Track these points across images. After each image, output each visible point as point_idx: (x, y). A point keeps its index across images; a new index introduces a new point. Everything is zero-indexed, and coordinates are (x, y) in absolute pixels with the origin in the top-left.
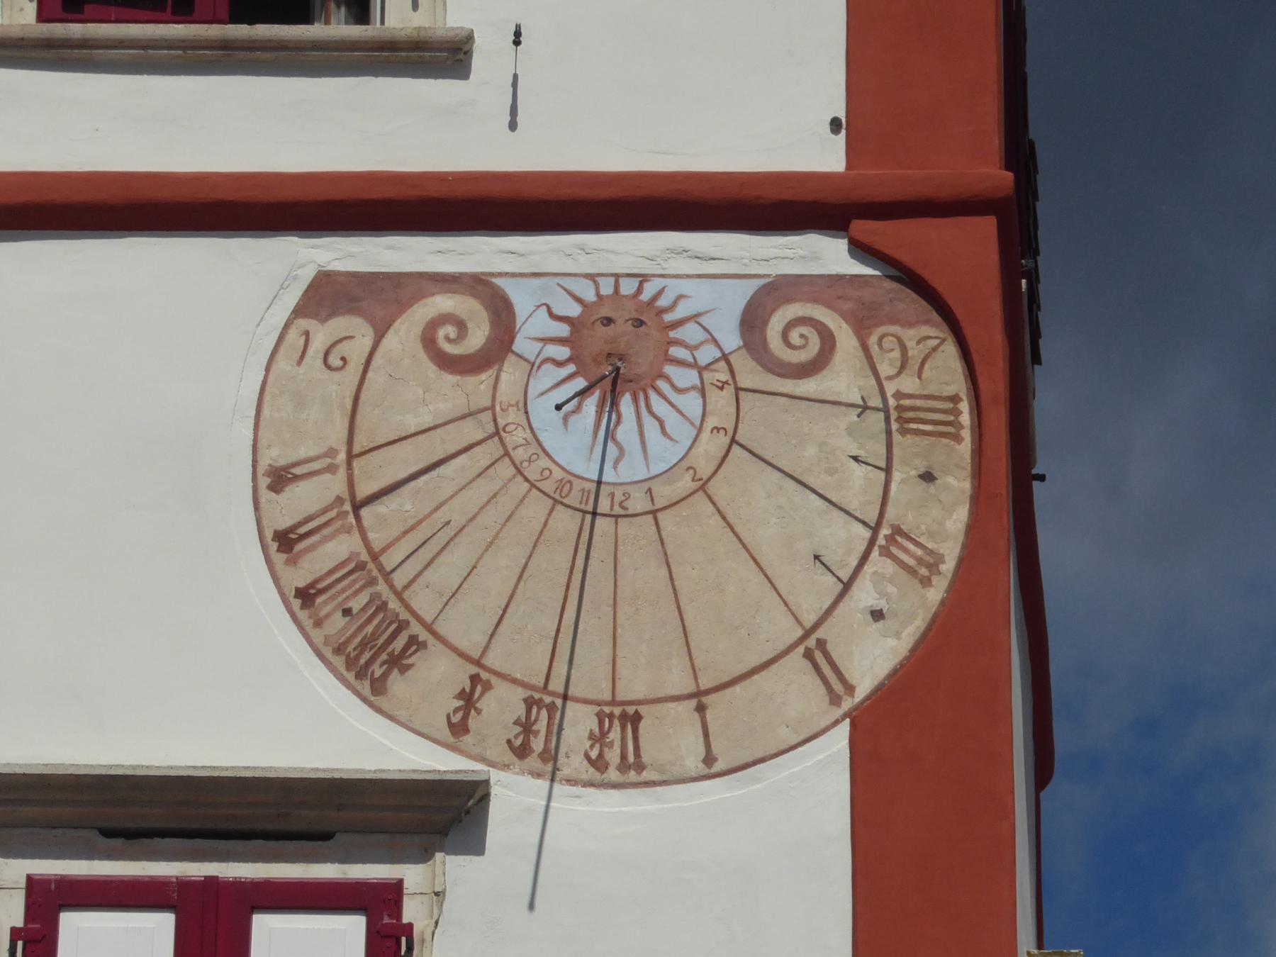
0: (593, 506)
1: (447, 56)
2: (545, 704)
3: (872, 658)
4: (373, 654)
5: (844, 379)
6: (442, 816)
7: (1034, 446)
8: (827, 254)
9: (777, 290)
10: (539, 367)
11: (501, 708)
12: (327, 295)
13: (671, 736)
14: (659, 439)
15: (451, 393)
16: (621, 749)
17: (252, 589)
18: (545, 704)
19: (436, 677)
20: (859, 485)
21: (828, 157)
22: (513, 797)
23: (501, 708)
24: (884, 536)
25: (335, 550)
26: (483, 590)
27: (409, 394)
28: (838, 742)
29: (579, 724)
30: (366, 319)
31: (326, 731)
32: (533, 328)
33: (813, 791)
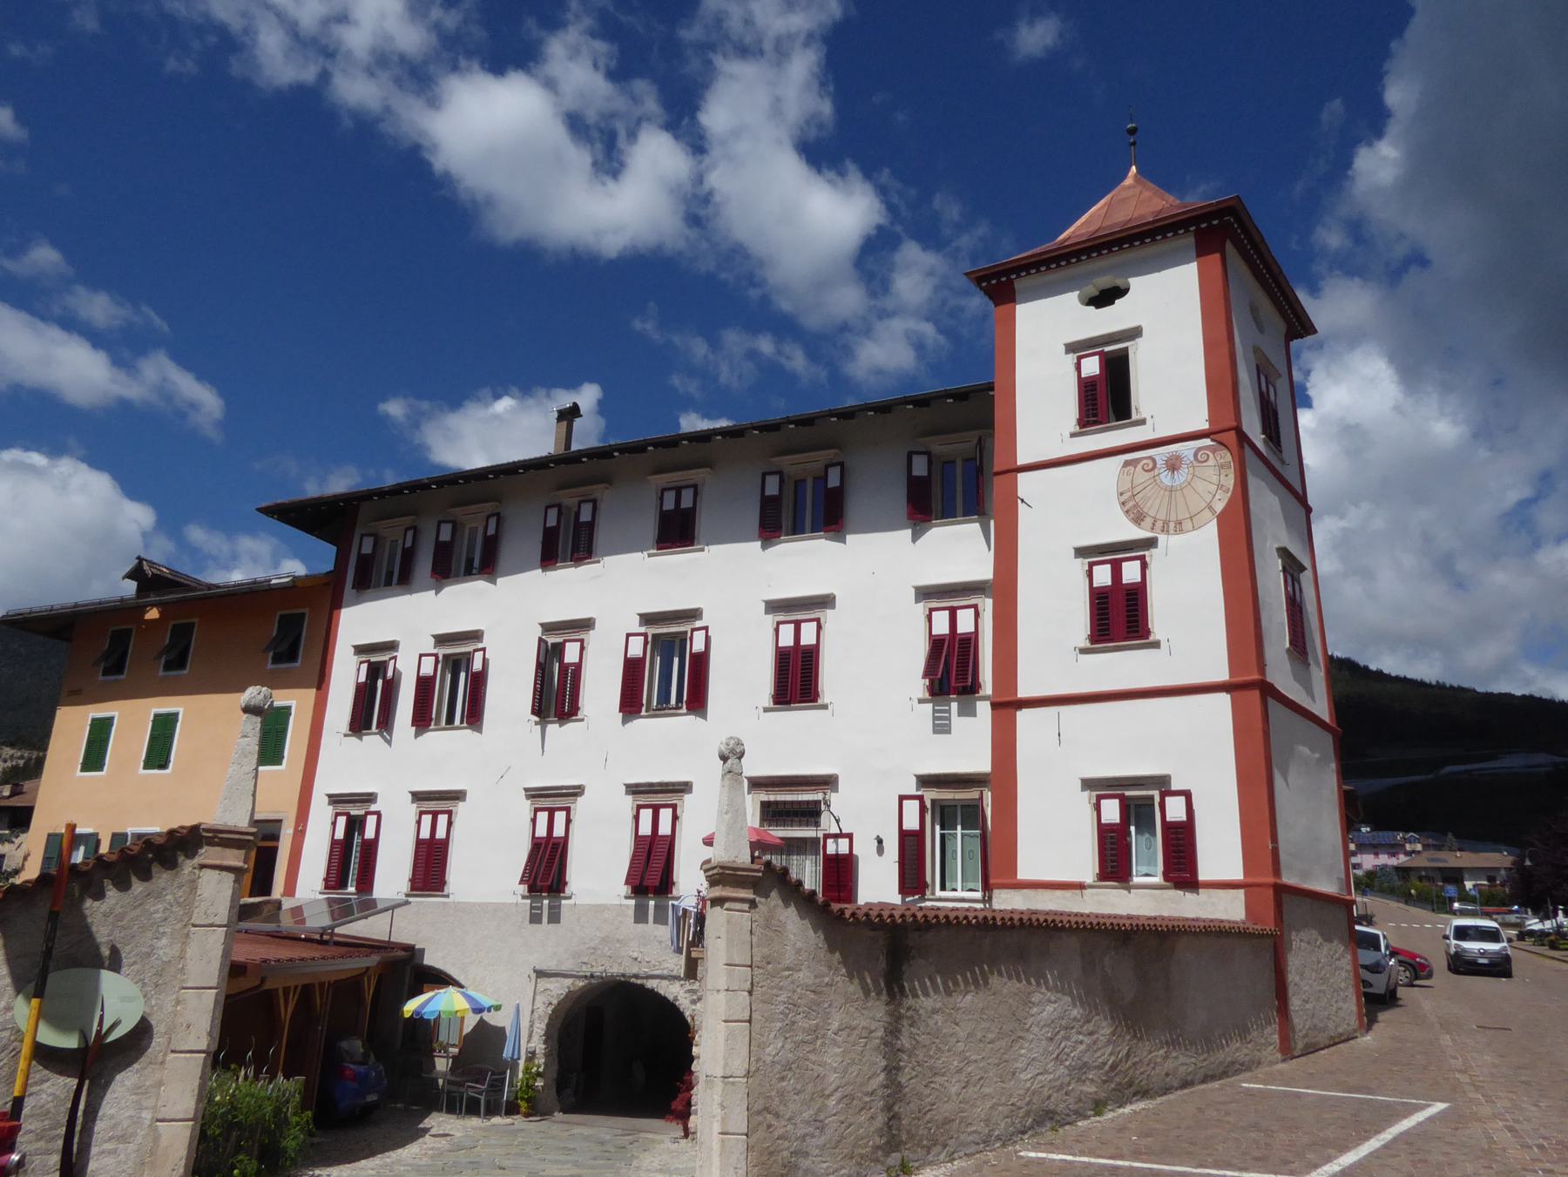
2: (1166, 523)
3: (1219, 507)
4: (1138, 519)
5: (1211, 462)
6: (1151, 543)
8: (1207, 442)
9: (1200, 449)
11: (1159, 524)
13: (1187, 525)
16: (1179, 528)
19: (1149, 521)
20: (1215, 479)
22: (1162, 539)
23: (1159, 524)
24: (1220, 486)
26: (1155, 506)
27: (1141, 477)
28: (1215, 521)
29: (1172, 525)
32: (1159, 462)
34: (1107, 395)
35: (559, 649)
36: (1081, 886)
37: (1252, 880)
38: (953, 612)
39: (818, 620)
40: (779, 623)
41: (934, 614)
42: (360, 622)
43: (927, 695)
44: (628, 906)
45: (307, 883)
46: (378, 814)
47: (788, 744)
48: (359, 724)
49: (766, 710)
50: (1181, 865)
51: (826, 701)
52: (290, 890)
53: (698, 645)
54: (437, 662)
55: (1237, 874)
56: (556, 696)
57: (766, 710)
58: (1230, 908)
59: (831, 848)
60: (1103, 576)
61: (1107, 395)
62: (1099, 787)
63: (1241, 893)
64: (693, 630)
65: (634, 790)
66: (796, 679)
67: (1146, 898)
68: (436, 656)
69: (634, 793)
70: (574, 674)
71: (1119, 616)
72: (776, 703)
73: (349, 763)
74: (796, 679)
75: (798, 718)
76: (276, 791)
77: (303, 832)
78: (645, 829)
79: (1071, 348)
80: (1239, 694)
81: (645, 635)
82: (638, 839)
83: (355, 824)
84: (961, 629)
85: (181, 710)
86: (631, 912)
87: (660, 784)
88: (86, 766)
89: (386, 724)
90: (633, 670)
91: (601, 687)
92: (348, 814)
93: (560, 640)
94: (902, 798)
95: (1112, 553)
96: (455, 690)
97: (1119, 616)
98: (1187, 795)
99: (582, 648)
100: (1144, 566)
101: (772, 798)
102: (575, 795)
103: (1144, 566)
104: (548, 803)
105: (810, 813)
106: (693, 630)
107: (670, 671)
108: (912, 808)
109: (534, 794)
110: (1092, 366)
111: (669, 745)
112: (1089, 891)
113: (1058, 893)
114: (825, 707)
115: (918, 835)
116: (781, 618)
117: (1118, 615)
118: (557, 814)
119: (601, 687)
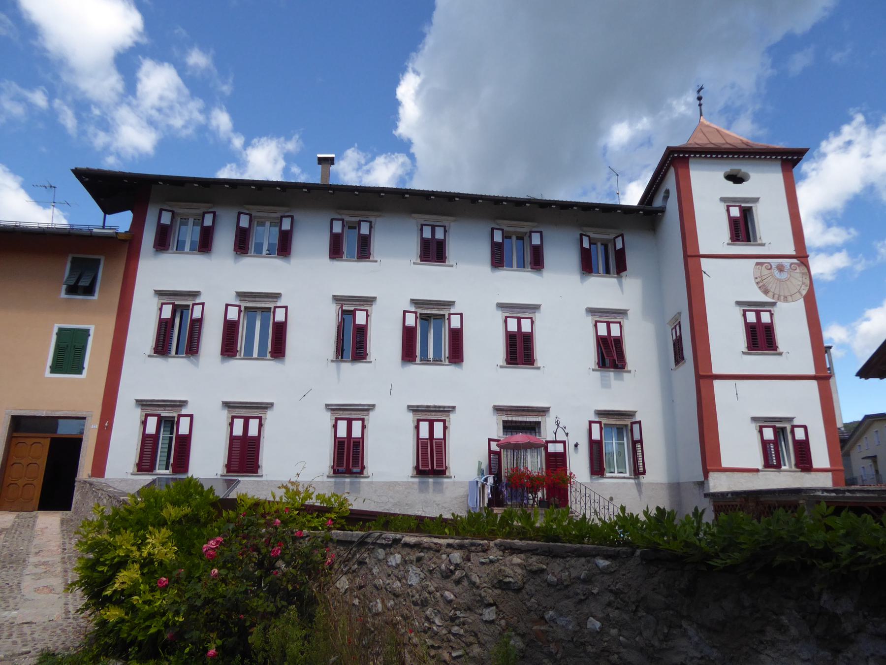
0: (780, 280)
1: (763, 245)
2: (779, 296)
3: (804, 293)
4: (766, 292)
5: (798, 271)
6: (773, 304)
7: (99, 170)
8: (795, 261)
9: (792, 264)
10: (13, 525)
11: (776, 296)
12: (757, 264)
13: (789, 299)
14: (784, 276)
15: (768, 272)
16: (786, 299)
17: (756, 287)
18: (779, 296)
19: (771, 294)
20: (800, 279)
21: (794, 253)
22: (779, 304)
23: (776, 296)
24: (803, 283)
25: (761, 284)
26: (772, 287)
27: (765, 272)
28: (802, 299)
29: (782, 298)
30: (176, 67)
31: (762, 298)
32: (774, 267)
33: (801, 302)
34: (742, 228)
35: (353, 313)
36: (757, 471)
37: (834, 468)
38: (519, 320)
39: (367, 311)
40: (506, 317)
41: (164, 306)
42: (159, 273)
43: (597, 367)
44: (413, 483)
45: (207, 462)
46: (639, 422)
47: (521, 388)
48: (162, 348)
49: (501, 367)
50: (804, 460)
51: (629, 369)
52: (99, 468)
53: (197, 314)
54: (240, 311)
55: (827, 465)
56: (352, 343)
57: (501, 367)
58: (825, 481)
59: (552, 448)
60: (751, 317)
61: (742, 228)
62: (762, 423)
63: (830, 474)
64: (275, 307)
65: (414, 409)
66: (520, 350)
67: (787, 478)
68: (239, 306)
69: (229, 407)
70: (361, 332)
71: (761, 338)
72: (508, 363)
73: (148, 377)
74: (520, 350)
75: (521, 373)
76: (68, 397)
77: (110, 428)
78: (238, 431)
79: (723, 200)
80: (822, 381)
81: (416, 313)
82: (232, 439)
83: (169, 424)
84: (613, 334)
85: (92, 329)
86: (416, 486)
87: (435, 407)
88: (58, 367)
89: (192, 348)
90: (408, 334)
91: (384, 340)
92: (159, 416)
93: (352, 308)
94: (591, 422)
95: (758, 307)
96: (261, 331)
97: (761, 338)
98: (805, 427)
99: (367, 316)
100: (772, 315)
101: (510, 419)
102: (266, 408)
103: (772, 315)
104: (432, 416)
105: (534, 428)
106: (194, 305)
107: (432, 336)
108: (596, 428)
109: (333, 409)
110: (735, 212)
111: (431, 382)
112: (760, 473)
113: (746, 474)
114: (539, 368)
115: (155, 438)
116: (508, 315)
117: (761, 337)
118: (251, 421)
119: (384, 340)
